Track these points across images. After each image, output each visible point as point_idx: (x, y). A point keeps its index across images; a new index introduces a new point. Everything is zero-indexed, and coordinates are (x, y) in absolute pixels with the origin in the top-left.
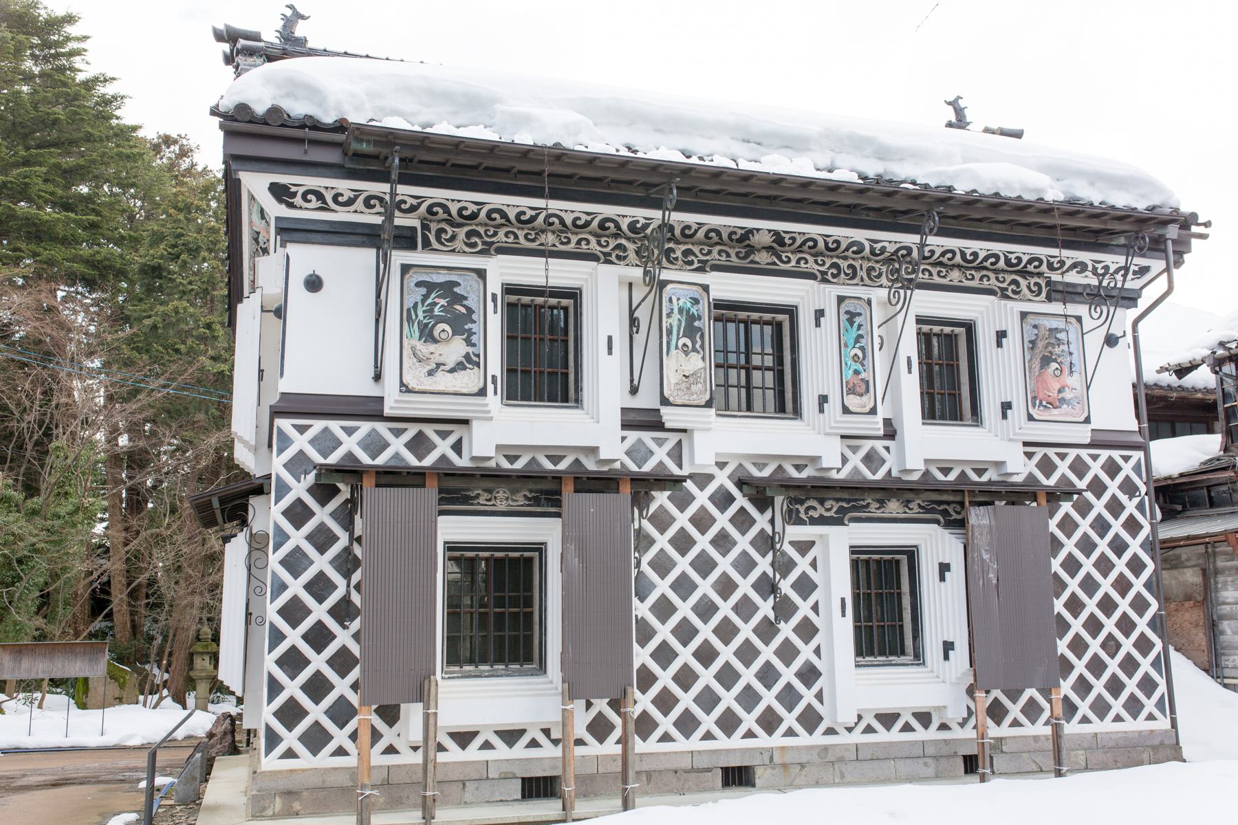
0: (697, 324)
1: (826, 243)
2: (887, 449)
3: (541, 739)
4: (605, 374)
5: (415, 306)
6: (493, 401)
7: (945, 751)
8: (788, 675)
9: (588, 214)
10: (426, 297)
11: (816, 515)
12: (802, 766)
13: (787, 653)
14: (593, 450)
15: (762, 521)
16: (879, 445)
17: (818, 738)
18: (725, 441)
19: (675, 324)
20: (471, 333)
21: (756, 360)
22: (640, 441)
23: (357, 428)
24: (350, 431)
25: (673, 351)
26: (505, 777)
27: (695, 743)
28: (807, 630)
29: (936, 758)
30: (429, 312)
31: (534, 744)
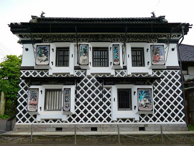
0: (86, 51)
1: (113, 36)
2: (125, 71)
3: (60, 121)
4: (72, 62)
5: (39, 51)
6: (90, 66)
7: (135, 126)
8: (105, 111)
9: (60, 35)
10: (40, 50)
11: (109, 83)
12: (106, 128)
13: (105, 108)
14: (69, 73)
15: (100, 85)
16: (124, 71)
17: (110, 123)
18: (93, 70)
19: (82, 51)
20: (47, 55)
21: (101, 57)
22: (165, 71)
23: (25, 71)
24: (24, 72)
25: (82, 56)
26: (53, 127)
27: (87, 123)
28: (108, 104)
29: (133, 127)
30: (41, 52)
31: (59, 122)
